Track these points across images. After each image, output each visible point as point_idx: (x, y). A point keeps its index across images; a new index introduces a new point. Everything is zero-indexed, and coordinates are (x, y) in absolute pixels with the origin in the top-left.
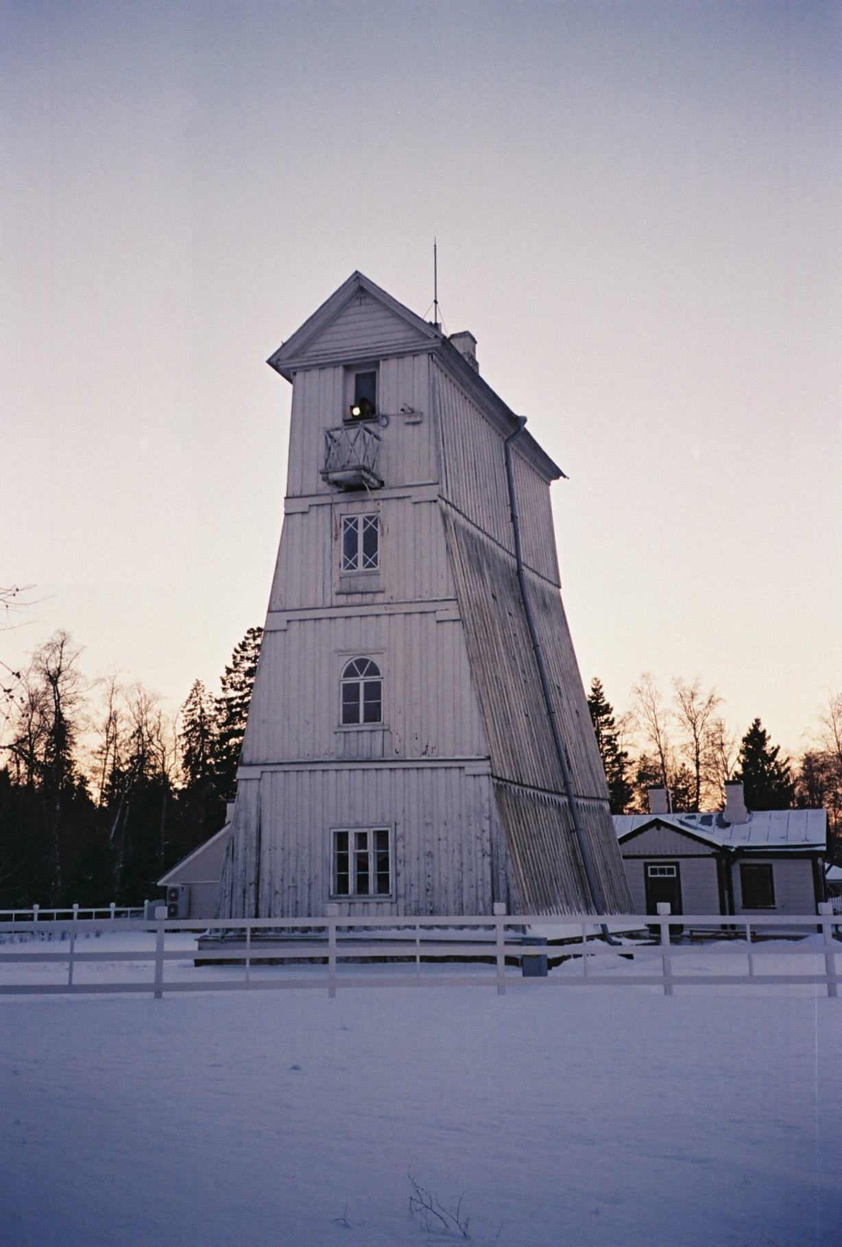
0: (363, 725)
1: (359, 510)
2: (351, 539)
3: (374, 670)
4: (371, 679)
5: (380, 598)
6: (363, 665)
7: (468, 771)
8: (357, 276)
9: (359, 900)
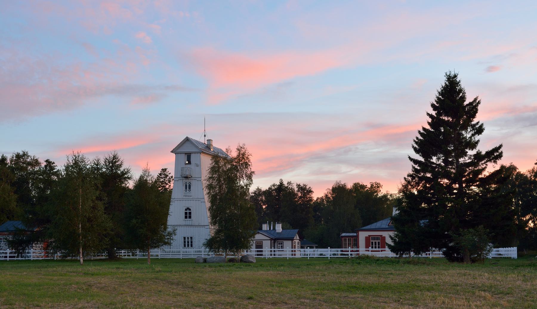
1: (188, 181)
2: (186, 186)
3: (190, 210)
6: (188, 209)
8: (187, 137)
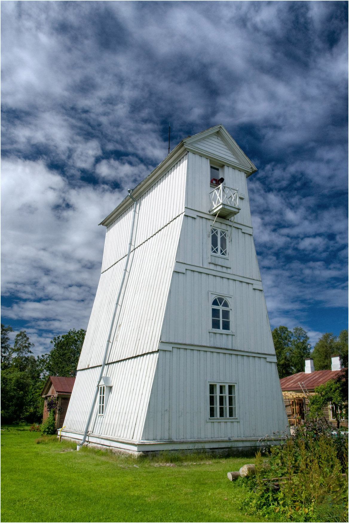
0: (221, 330)
3: (226, 305)
4: (225, 308)
5: (229, 271)
7: (268, 360)
9: (222, 420)
